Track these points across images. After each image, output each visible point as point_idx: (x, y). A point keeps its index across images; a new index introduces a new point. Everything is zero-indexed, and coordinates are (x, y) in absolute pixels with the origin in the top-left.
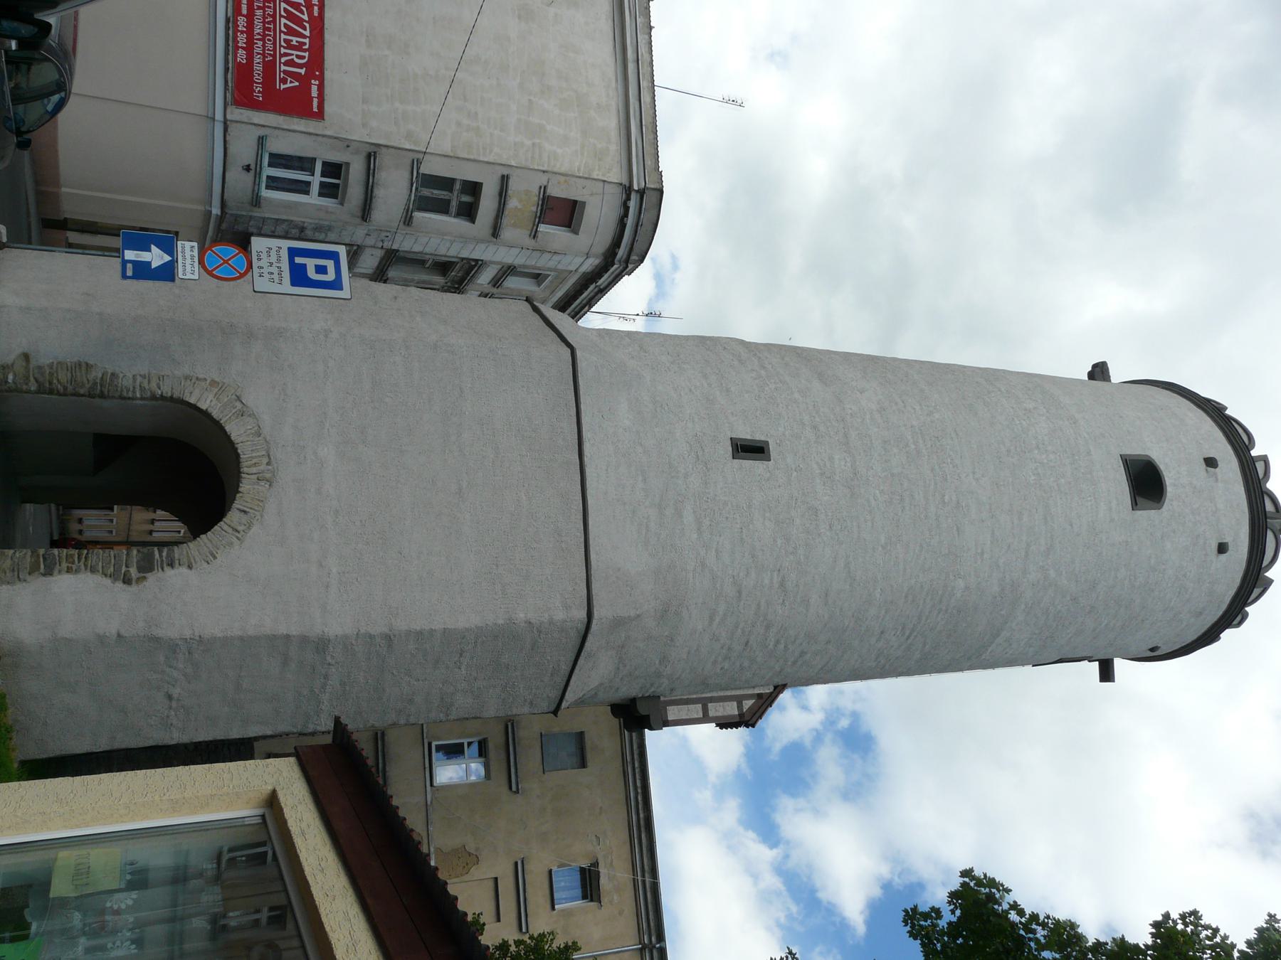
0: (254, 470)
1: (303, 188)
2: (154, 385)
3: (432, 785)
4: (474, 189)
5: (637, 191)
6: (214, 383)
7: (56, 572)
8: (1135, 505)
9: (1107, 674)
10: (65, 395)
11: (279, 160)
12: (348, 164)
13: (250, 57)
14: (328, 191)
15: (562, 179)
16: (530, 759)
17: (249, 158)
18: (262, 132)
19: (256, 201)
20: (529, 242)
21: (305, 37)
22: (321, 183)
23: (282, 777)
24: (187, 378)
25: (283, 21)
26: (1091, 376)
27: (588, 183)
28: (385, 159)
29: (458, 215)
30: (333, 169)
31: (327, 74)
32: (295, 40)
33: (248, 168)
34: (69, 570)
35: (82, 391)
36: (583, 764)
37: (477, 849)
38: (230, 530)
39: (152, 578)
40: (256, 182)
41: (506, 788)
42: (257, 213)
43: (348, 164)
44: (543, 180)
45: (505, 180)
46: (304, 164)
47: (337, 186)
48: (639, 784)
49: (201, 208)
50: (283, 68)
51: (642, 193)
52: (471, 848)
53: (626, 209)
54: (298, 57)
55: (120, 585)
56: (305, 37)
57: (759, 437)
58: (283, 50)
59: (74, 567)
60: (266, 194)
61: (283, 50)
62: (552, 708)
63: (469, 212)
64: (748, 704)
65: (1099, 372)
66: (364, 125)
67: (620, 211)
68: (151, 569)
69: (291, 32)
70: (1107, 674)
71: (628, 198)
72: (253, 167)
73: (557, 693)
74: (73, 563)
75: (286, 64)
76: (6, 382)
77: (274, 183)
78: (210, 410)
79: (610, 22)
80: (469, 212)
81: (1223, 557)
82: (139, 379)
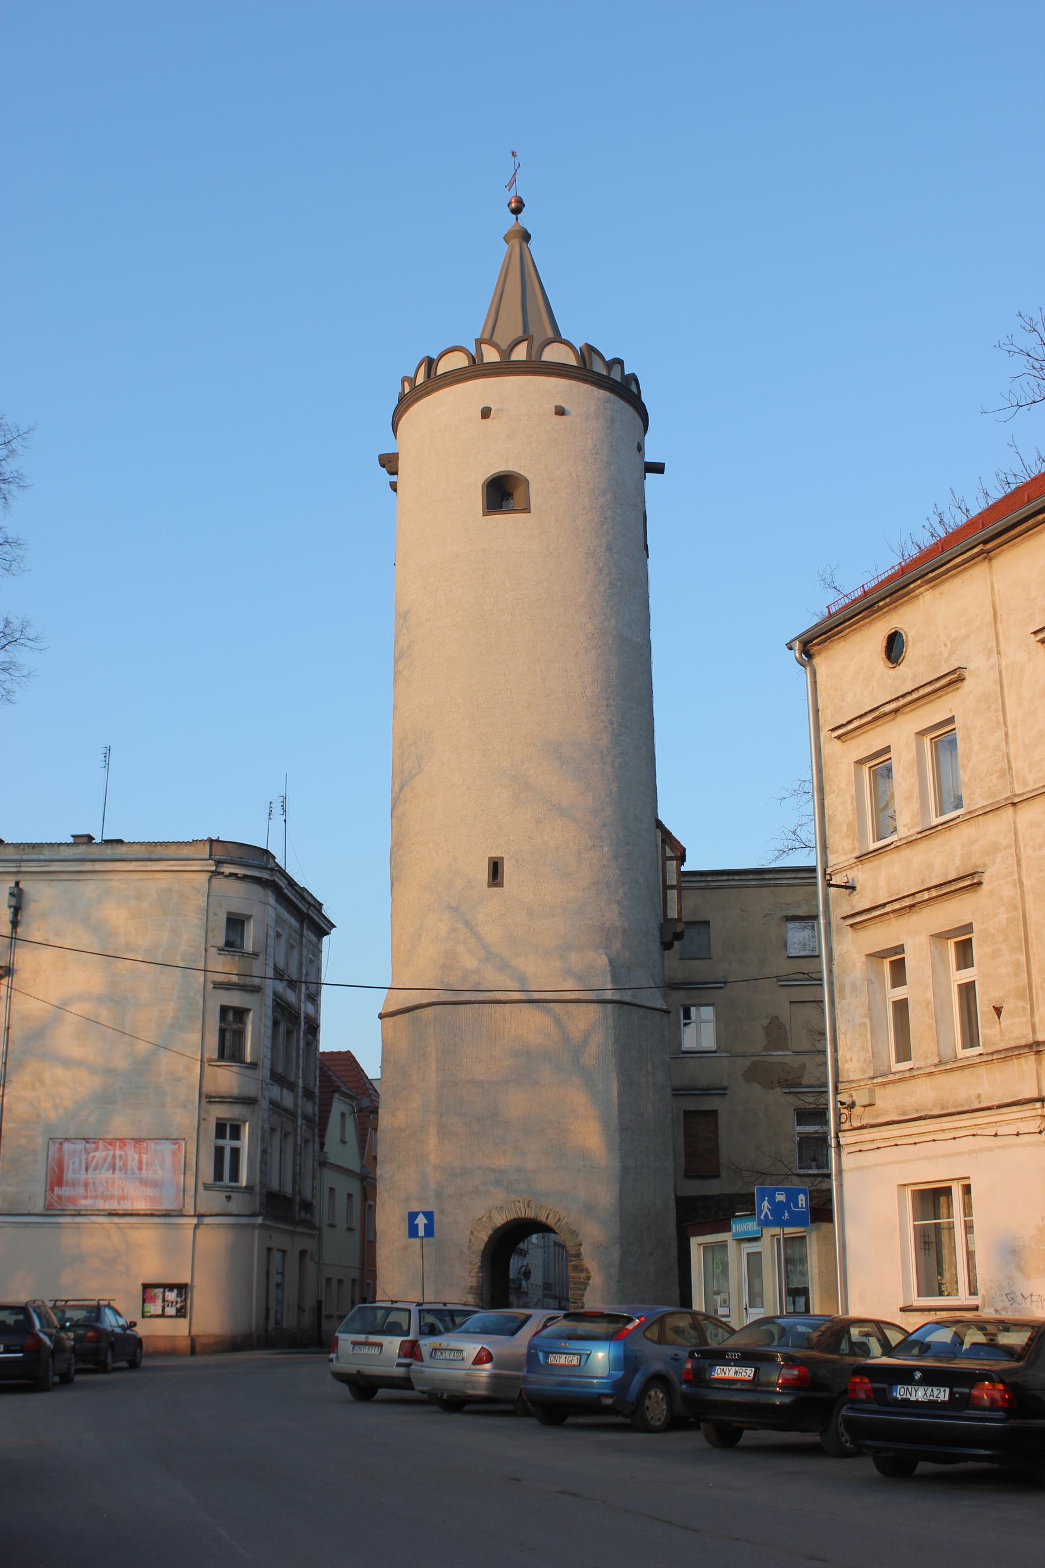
1: (236, 1152)
2: (476, 1267)
3: (715, 1052)
4: (224, 1010)
5: (217, 866)
6: (472, 1233)
8: (527, 510)
9: (657, 468)
11: (218, 1175)
12: (218, 1119)
14: (236, 1134)
15: (210, 934)
16: (699, 969)
17: (221, 1196)
18: (201, 1187)
19: (249, 1189)
20: (262, 957)
21: (114, 1156)
22: (231, 1138)
24: (470, 1248)
27: (212, 910)
28: (210, 1088)
30: (221, 1129)
32: (118, 1163)
33: (229, 1198)
36: (707, 923)
37: (767, 1017)
40: (238, 1189)
41: (721, 991)
42: (258, 1188)
43: (218, 1119)
44: (213, 951)
45: (218, 986)
46: (219, 1151)
47: (231, 1126)
48: (725, 878)
49: (257, 1232)
50: (144, 1171)
51: (219, 863)
52: (765, 1022)
53: (231, 875)
55: (590, 1282)
56: (114, 1156)
60: (243, 1181)
62: (666, 1015)
63: (240, 1014)
64: (669, 853)
70: (657, 468)
72: (228, 1194)
73: (657, 1014)
77: (235, 1176)
79: (56, 883)
80: (240, 1014)
81: (567, 407)
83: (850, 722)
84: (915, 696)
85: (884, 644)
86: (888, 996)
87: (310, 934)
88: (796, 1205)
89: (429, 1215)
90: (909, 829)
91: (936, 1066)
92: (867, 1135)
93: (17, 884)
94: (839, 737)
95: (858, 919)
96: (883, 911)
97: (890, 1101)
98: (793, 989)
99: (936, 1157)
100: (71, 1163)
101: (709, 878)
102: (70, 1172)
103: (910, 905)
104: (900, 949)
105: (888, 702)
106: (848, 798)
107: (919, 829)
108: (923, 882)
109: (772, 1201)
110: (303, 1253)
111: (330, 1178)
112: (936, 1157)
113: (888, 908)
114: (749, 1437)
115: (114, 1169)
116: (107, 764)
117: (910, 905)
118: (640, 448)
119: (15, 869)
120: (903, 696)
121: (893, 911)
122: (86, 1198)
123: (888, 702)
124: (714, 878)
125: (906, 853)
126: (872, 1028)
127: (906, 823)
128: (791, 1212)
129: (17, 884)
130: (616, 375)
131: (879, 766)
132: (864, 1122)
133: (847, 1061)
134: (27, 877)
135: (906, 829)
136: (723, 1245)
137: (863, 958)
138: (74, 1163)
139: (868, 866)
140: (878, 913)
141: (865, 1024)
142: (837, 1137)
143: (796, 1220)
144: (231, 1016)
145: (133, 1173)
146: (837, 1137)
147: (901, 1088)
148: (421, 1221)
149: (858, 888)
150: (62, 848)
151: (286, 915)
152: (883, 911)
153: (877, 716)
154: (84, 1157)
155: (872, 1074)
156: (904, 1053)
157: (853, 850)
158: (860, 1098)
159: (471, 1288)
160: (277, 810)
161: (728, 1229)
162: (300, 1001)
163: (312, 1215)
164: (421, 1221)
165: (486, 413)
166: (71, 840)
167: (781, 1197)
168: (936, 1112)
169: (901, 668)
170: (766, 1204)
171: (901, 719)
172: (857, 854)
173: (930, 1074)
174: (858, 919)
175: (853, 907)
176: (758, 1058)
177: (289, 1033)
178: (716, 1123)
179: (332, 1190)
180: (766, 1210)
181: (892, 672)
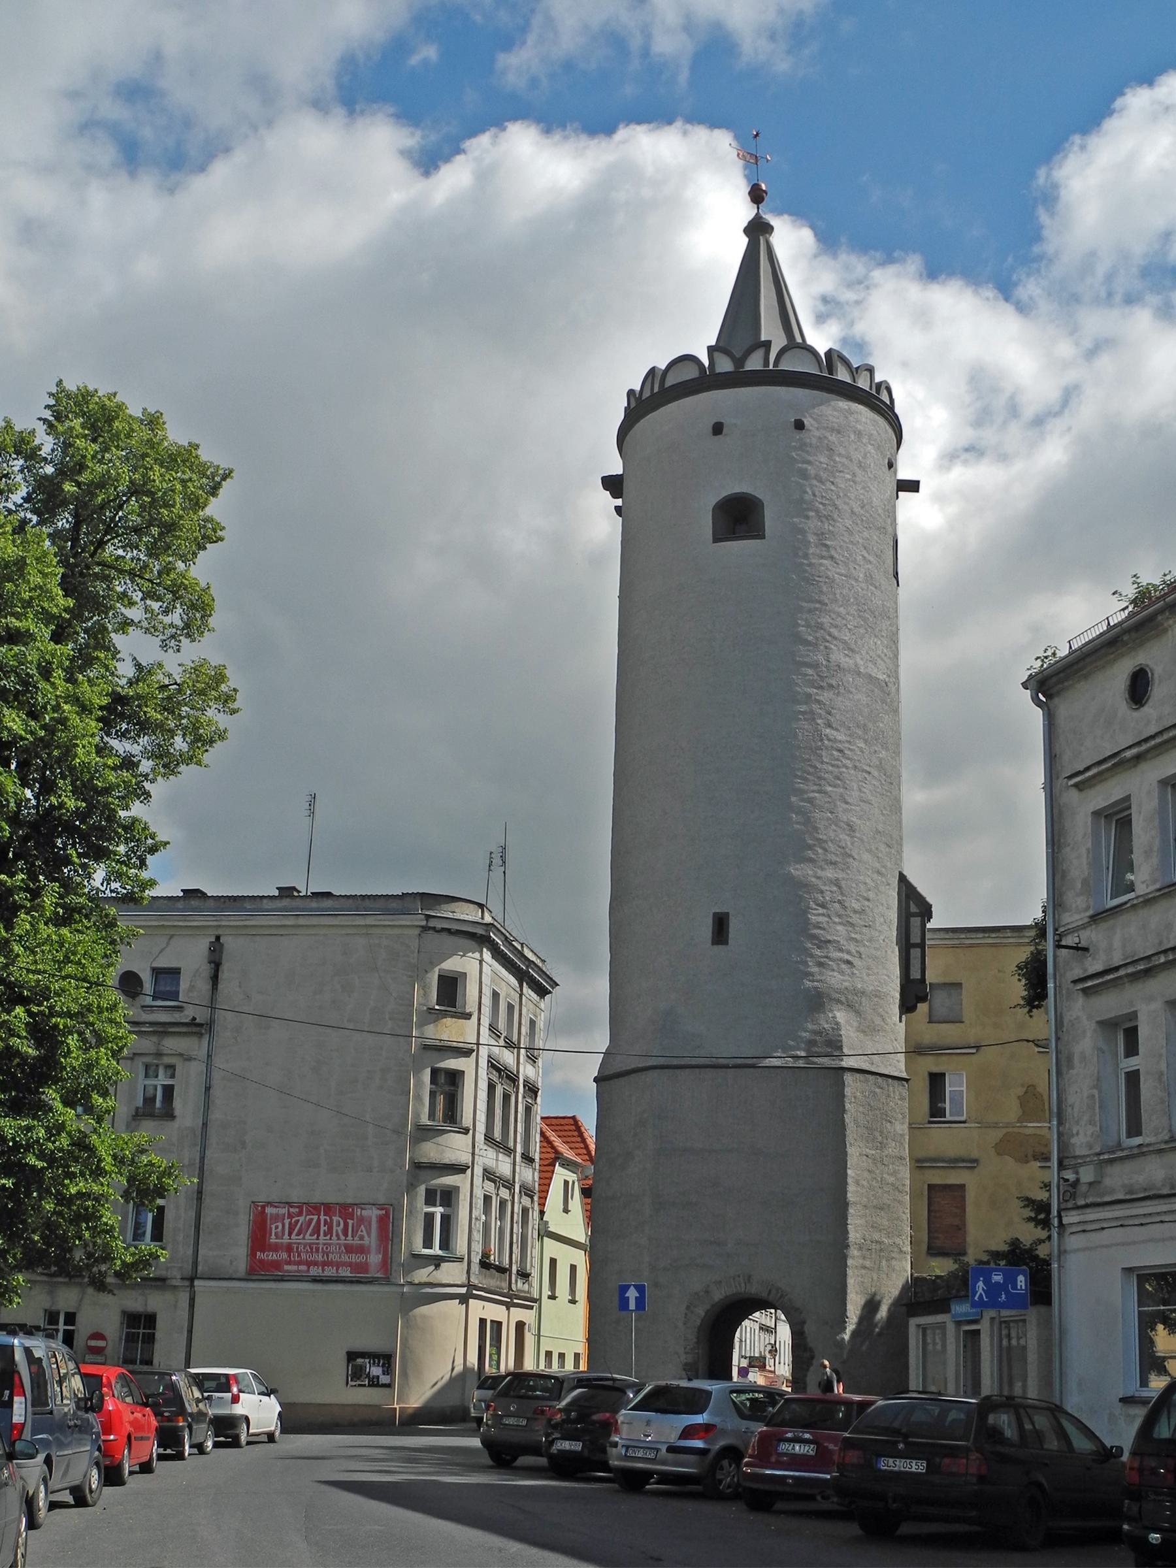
6: (688, 1308)
9: (912, 486)
13: (345, 1264)
21: (319, 1220)
23: (913, 1322)
25: (307, 1236)
26: (616, 494)
31: (349, 1201)
32: (323, 1228)
36: (960, 984)
37: (1022, 1086)
50: (350, 1237)
52: (1020, 1091)
53: (443, 930)
54: (338, 1225)
56: (319, 1220)
57: (710, 921)
58: (334, 1237)
61: (334, 1237)
64: (914, 909)
65: (613, 484)
66: (392, 1171)
67: (444, 935)
69: (317, 1231)
70: (912, 486)
71: (434, 929)
75: (346, 1235)
77: (445, 1244)
83: (1088, 769)
84: (1158, 740)
85: (1128, 683)
86: (1122, 1065)
87: (532, 994)
88: (1015, 1287)
89: (640, 1289)
90: (1147, 886)
91: (1166, 1142)
92: (1092, 1214)
93: (218, 938)
94: (1076, 785)
95: (1090, 984)
96: (1116, 975)
97: (1118, 1179)
98: (965, 1057)
99: (1163, 1240)
100: (273, 1227)
101: (963, 936)
102: (273, 1236)
103: (1145, 969)
104: (1134, 1016)
105: (1130, 747)
106: (1083, 851)
107: (1158, 886)
108: (1161, 943)
109: (987, 1282)
110: (520, 1326)
111: (552, 1248)
112: (1163, 1240)
113: (1122, 972)
114: (779, 1506)
115: (319, 1236)
116: (312, 813)
117: (1145, 969)
118: (891, 465)
119: (215, 923)
120: (1146, 740)
121: (1127, 975)
122: (289, 1263)
123: (1130, 747)
124: (968, 935)
125: (1143, 913)
126: (1101, 1101)
127: (1143, 878)
128: (1007, 1293)
129: (218, 938)
130: (863, 383)
131: (1118, 818)
132: (1090, 1200)
133: (1073, 1136)
134: (228, 931)
135: (1144, 886)
136: (942, 1326)
137: (1094, 1025)
138: (277, 1227)
139: (1104, 926)
140: (1111, 976)
141: (1093, 1096)
142: (1060, 1217)
143: (1015, 1302)
144: (442, 1079)
145: (339, 1239)
146: (1060, 1217)
147: (1128, 1166)
148: (632, 1294)
149: (1091, 951)
150: (265, 901)
151: (504, 972)
152: (1116, 975)
153: (1119, 763)
154: (287, 1221)
155: (1098, 1150)
156: (1135, 1128)
157: (1088, 908)
158: (1087, 1175)
159: (686, 1364)
160: (497, 861)
161: (946, 1309)
162: (518, 1063)
163: (530, 1286)
164: (632, 1294)
165: (718, 429)
166: (181, 894)
167: (997, 1278)
168: (1165, 1191)
169: (1146, 709)
170: (981, 1284)
171: (1144, 766)
172: (1091, 912)
173: (1160, 1151)
174: (1090, 984)
175: (1086, 970)
176: (1010, 1130)
177: (506, 1097)
178: (963, 1198)
179: (553, 1262)
180: (981, 1291)
181: (1136, 714)
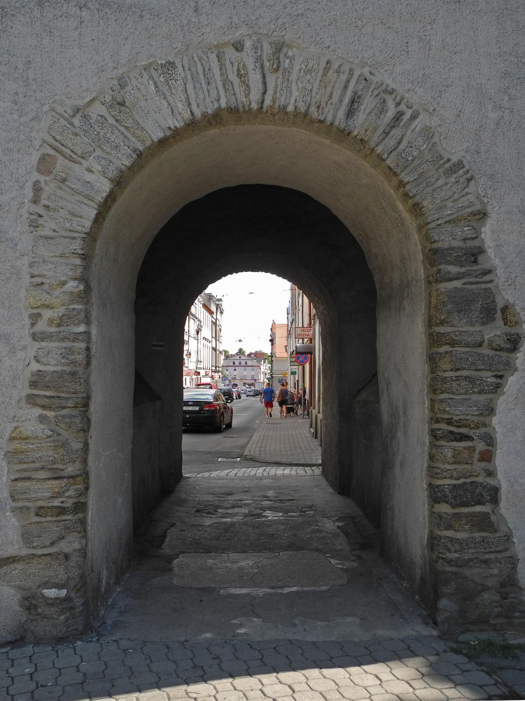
0: (255, 78)
6: (45, 165)
7: (491, 481)
10: (86, 475)
29: (432, 514)
34: (487, 457)
35: (76, 445)
38: (396, 132)
39: (506, 295)
59: (481, 446)
68: (489, 296)
74: (472, 449)
76: (67, 599)
78: (112, 172)
82: (41, 326)
